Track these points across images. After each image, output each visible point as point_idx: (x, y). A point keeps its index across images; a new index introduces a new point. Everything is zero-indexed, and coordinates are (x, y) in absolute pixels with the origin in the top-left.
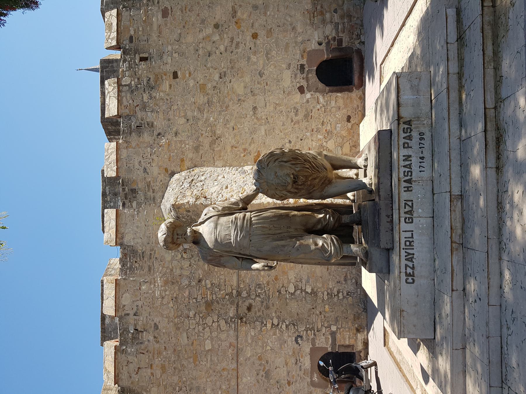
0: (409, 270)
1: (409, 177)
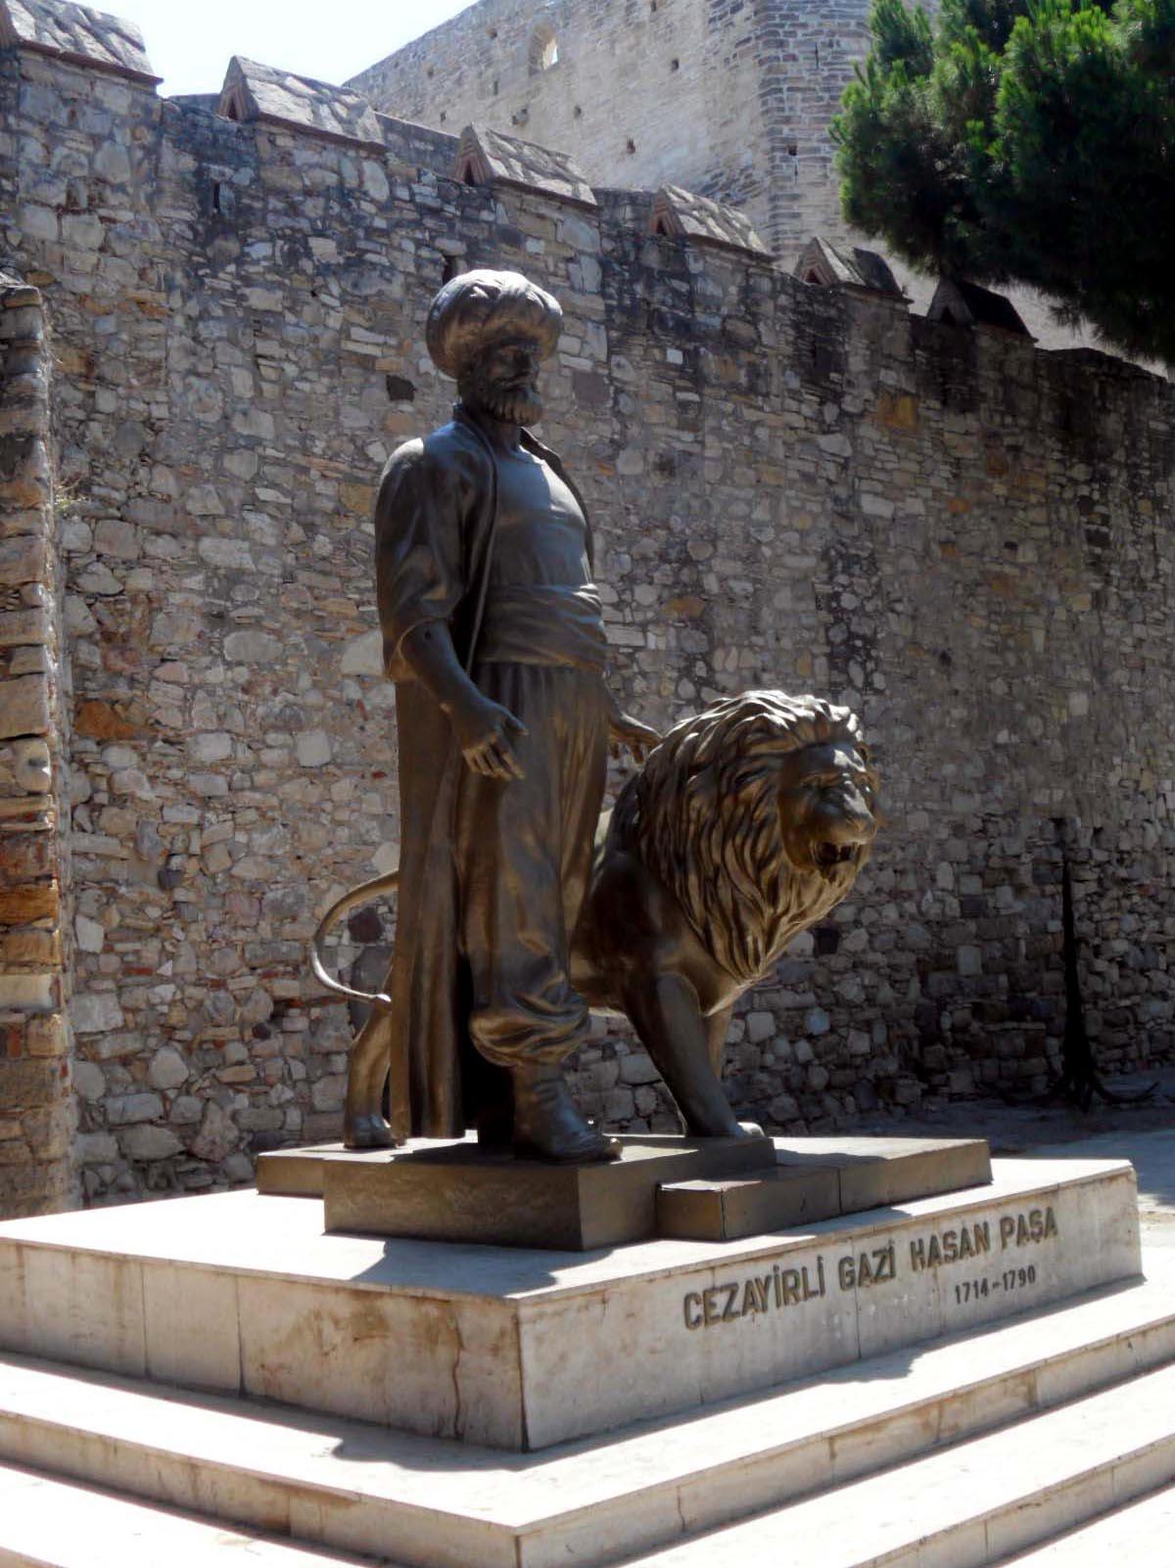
0: (721, 1299)
1: (943, 1252)
